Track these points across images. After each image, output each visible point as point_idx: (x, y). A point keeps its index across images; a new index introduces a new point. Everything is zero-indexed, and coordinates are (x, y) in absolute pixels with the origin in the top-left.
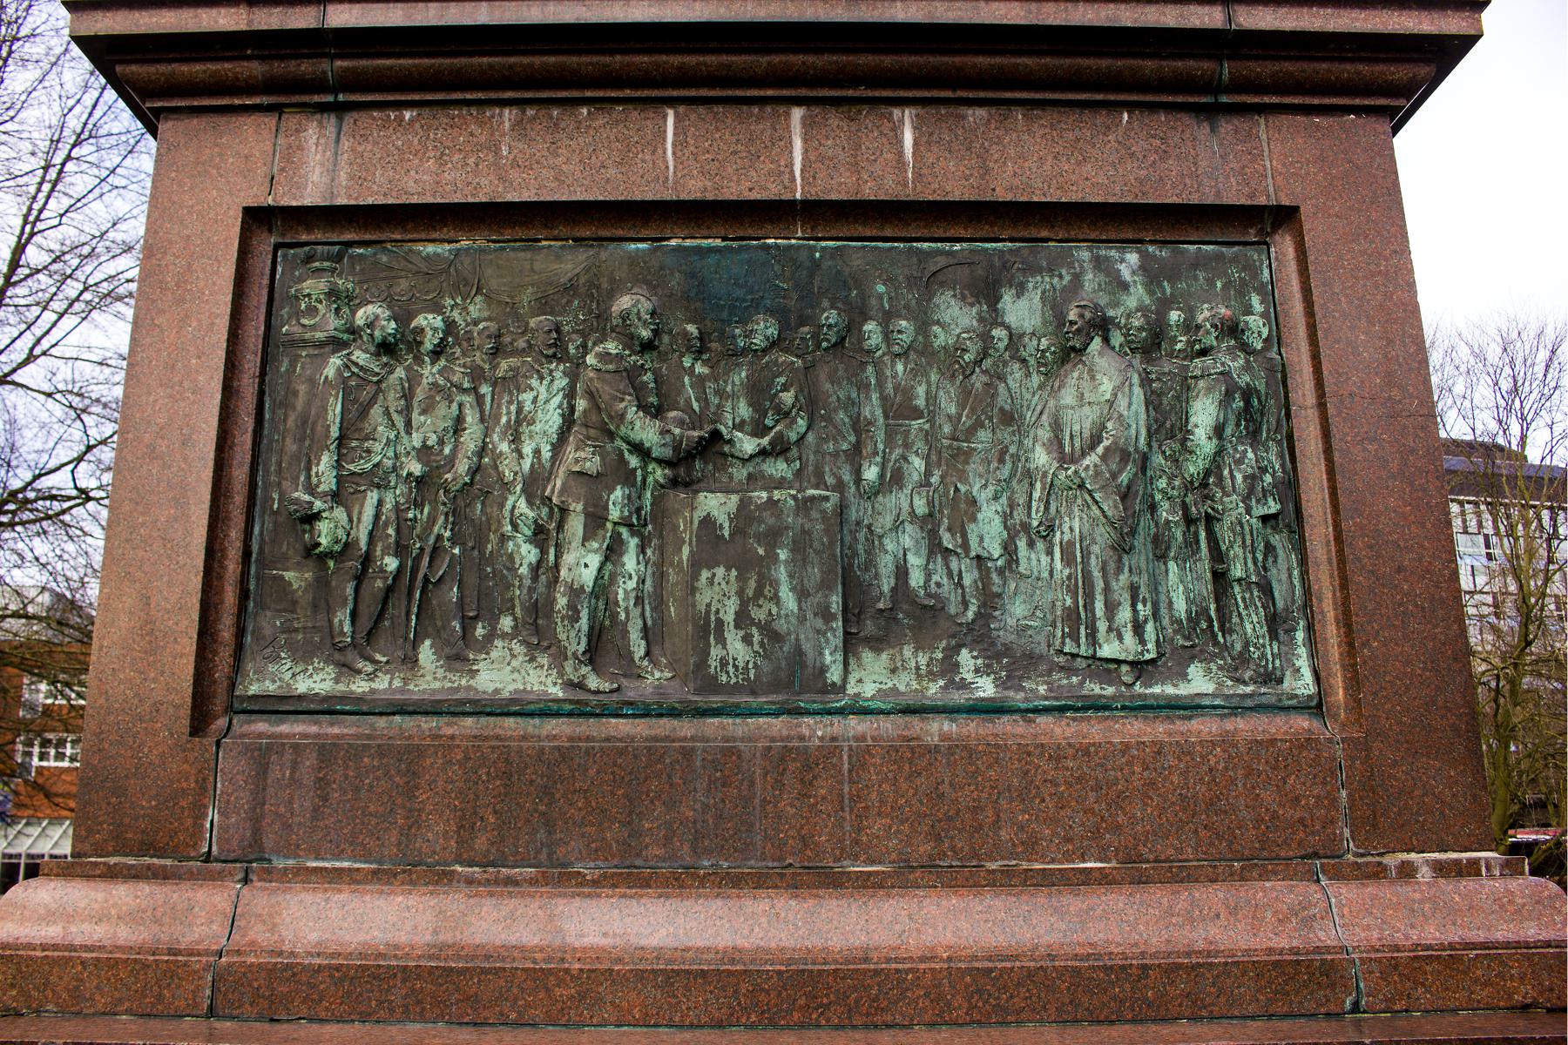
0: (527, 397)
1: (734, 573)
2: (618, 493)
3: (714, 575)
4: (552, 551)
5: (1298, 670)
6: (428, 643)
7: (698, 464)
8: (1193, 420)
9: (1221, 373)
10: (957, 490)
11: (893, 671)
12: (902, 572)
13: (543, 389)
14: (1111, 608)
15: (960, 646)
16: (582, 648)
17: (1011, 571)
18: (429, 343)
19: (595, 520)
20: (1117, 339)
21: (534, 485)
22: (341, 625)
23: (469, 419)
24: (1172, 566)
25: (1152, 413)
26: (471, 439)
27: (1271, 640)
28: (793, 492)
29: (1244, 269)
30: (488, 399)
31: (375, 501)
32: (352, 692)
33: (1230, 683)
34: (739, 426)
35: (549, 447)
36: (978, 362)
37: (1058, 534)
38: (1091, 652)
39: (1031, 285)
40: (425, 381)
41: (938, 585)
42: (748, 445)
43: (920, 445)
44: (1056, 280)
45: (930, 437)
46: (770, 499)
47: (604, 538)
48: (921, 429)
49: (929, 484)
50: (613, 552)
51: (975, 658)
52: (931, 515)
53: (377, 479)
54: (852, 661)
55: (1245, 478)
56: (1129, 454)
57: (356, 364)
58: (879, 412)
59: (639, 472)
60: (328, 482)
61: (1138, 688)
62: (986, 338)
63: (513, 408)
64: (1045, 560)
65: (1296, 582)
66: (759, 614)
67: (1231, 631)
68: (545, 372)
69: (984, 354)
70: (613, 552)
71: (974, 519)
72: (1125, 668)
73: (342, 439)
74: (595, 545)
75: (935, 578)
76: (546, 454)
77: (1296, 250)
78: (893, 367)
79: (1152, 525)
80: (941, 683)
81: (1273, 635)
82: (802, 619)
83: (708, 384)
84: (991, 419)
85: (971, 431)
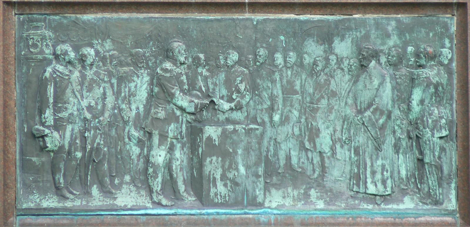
0: (132, 85)
1: (220, 159)
2: (172, 126)
3: (212, 160)
4: (146, 149)
5: (450, 200)
6: (95, 186)
7: (204, 113)
8: (412, 97)
9: (425, 78)
10: (312, 124)
11: (284, 197)
12: (288, 158)
13: (139, 82)
14: (373, 173)
15: (310, 188)
16: (159, 189)
17: (333, 157)
18: (89, 61)
19: (163, 137)
20: (383, 59)
21: (138, 123)
22: (59, 179)
23: (108, 94)
24: (401, 156)
25: (396, 92)
26: (110, 100)
27: (439, 187)
28: (244, 126)
29: (443, 27)
30: (115, 85)
31: (70, 129)
32: (66, 207)
33: (421, 204)
34: (222, 98)
35: (142, 106)
36: (323, 70)
37: (353, 143)
38: (364, 191)
39: (347, 36)
40: (88, 78)
41: (303, 163)
42: (226, 106)
43: (297, 106)
44: (358, 34)
45: (302, 103)
46: (234, 129)
47: (167, 144)
48: (297, 99)
49: (301, 122)
50: (171, 149)
51: (317, 192)
52: (301, 134)
53: (70, 120)
54: (267, 193)
55: (433, 121)
56: (384, 112)
57: (58, 71)
58: (280, 92)
59: (180, 117)
60: (50, 121)
61: (383, 206)
62: (327, 59)
63: (127, 90)
64: (347, 153)
65: (453, 163)
66: (230, 175)
67: (424, 183)
68: (139, 74)
69: (326, 67)
70: (171, 149)
71: (318, 136)
72: (378, 197)
73: (55, 102)
74: (163, 147)
75: (302, 160)
76: (141, 108)
77: (65, 224)
78: (286, 72)
79: (393, 139)
80: (303, 202)
81: (440, 185)
82: (247, 177)
83: (209, 80)
84: (327, 95)
85: (319, 100)
